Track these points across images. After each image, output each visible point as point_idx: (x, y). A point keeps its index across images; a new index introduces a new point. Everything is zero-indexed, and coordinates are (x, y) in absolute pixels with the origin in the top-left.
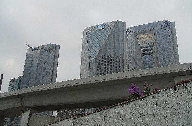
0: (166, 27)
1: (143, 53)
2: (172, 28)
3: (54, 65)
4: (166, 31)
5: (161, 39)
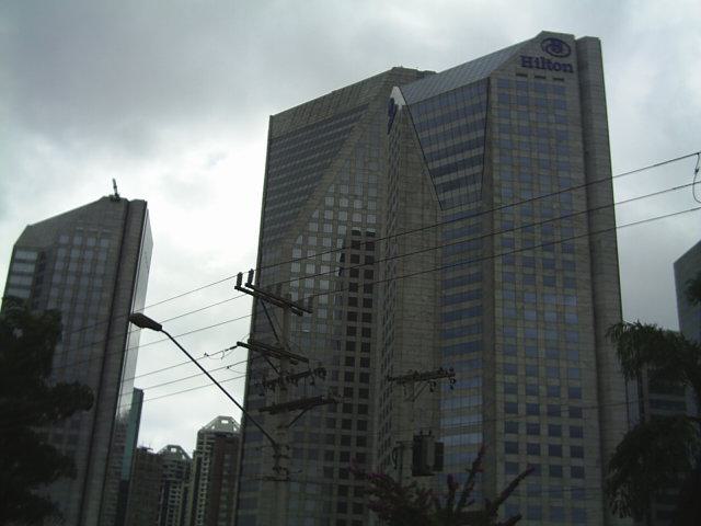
0: (546, 65)
1: (438, 180)
3: (116, 283)
5: (515, 123)
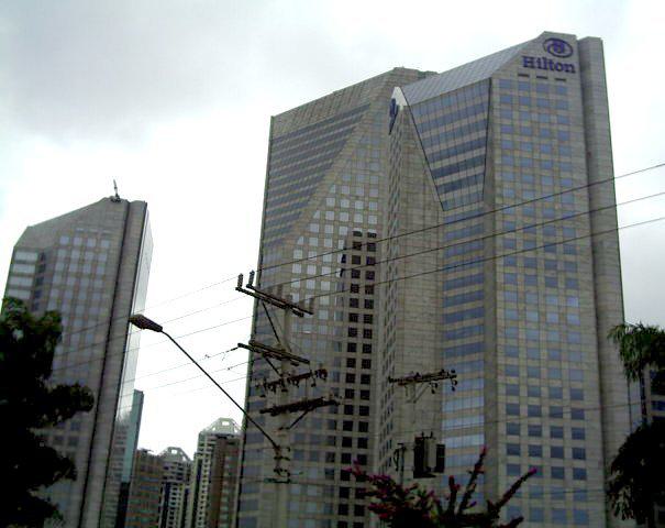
0: (548, 65)
1: (440, 181)
2: (584, 67)
4: (551, 82)
